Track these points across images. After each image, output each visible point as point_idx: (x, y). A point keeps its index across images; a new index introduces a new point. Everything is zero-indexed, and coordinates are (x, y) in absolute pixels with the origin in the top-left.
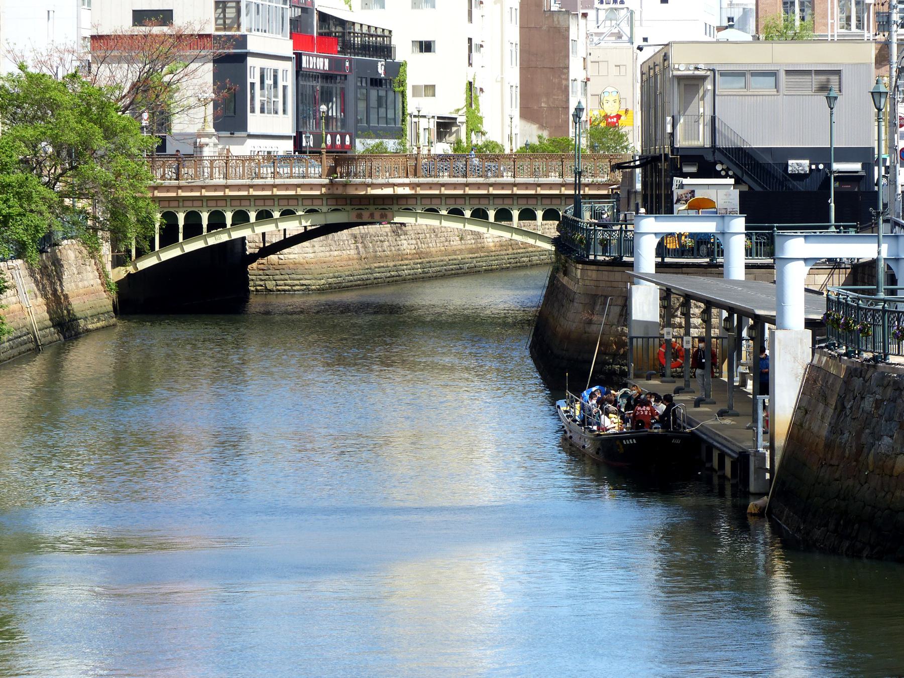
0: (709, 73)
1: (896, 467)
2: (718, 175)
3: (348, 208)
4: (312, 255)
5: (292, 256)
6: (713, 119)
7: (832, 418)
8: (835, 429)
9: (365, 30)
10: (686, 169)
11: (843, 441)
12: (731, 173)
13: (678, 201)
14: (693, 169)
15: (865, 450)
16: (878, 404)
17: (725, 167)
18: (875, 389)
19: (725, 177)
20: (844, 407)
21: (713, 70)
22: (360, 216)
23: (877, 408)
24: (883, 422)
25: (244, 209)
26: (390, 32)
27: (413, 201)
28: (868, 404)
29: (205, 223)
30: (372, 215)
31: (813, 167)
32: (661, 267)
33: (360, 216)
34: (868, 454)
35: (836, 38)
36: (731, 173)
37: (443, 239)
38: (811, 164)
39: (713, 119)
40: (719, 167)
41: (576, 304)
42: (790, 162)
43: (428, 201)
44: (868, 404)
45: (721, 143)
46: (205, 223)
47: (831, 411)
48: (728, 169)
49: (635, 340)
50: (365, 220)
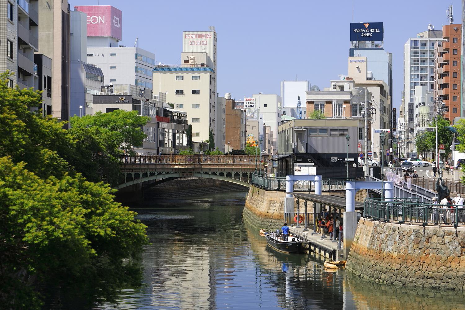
0: (305, 129)
1: (394, 256)
2: (308, 162)
3: (180, 172)
4: (164, 187)
5: (157, 188)
6: (307, 144)
7: (370, 240)
8: (371, 243)
9: (183, 115)
10: (298, 160)
11: (375, 247)
12: (312, 161)
13: (296, 170)
14: (301, 160)
15: (383, 251)
16: (387, 236)
17: (310, 160)
18: (386, 231)
19: (311, 163)
20: (374, 237)
21: (307, 129)
22: (183, 175)
23: (386, 237)
24: (389, 241)
25: (223, 172)
26: (186, 115)
27: (200, 170)
28: (383, 236)
29: (133, 176)
30: (187, 174)
31: (339, 160)
32: (344, 192)
33: (183, 175)
34: (384, 252)
35: (309, 118)
36: (312, 161)
37: (203, 182)
38: (338, 159)
39: (307, 144)
40: (309, 160)
41: (264, 203)
42: (331, 158)
43: (205, 170)
44: (383, 236)
45: (309, 152)
46: (133, 176)
47: (369, 238)
48: (311, 161)
49: (310, 214)
50: (185, 176)
